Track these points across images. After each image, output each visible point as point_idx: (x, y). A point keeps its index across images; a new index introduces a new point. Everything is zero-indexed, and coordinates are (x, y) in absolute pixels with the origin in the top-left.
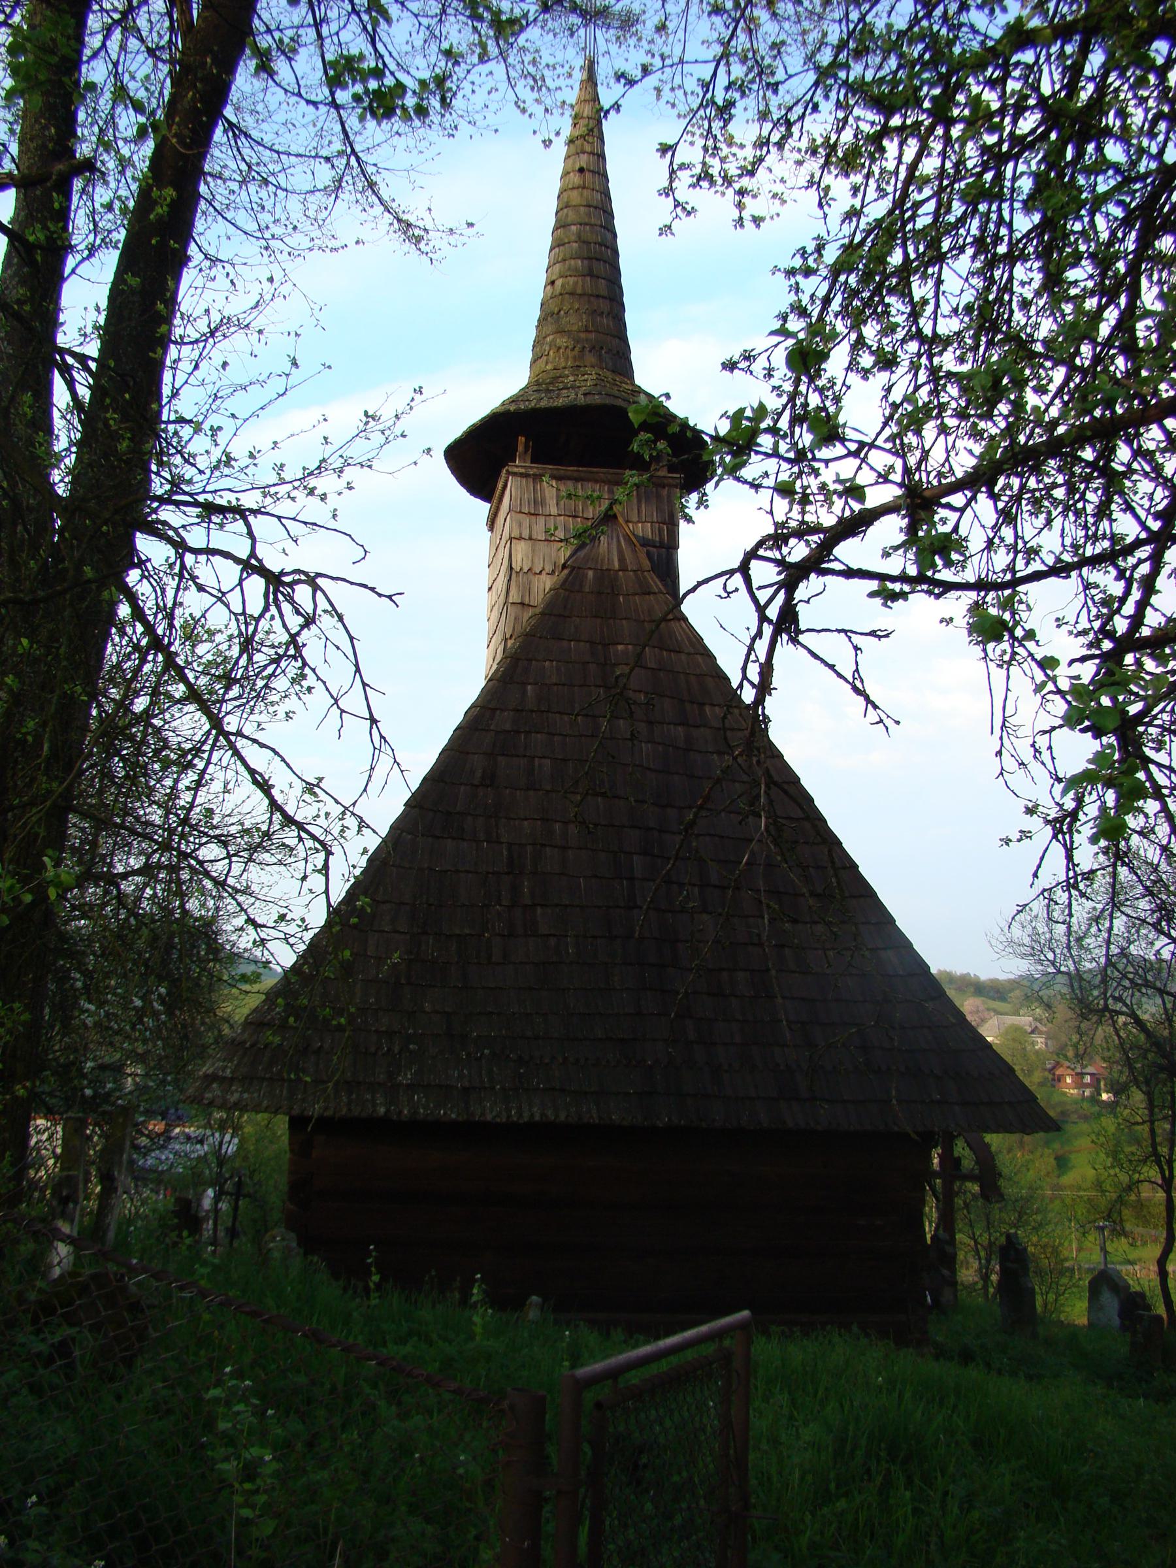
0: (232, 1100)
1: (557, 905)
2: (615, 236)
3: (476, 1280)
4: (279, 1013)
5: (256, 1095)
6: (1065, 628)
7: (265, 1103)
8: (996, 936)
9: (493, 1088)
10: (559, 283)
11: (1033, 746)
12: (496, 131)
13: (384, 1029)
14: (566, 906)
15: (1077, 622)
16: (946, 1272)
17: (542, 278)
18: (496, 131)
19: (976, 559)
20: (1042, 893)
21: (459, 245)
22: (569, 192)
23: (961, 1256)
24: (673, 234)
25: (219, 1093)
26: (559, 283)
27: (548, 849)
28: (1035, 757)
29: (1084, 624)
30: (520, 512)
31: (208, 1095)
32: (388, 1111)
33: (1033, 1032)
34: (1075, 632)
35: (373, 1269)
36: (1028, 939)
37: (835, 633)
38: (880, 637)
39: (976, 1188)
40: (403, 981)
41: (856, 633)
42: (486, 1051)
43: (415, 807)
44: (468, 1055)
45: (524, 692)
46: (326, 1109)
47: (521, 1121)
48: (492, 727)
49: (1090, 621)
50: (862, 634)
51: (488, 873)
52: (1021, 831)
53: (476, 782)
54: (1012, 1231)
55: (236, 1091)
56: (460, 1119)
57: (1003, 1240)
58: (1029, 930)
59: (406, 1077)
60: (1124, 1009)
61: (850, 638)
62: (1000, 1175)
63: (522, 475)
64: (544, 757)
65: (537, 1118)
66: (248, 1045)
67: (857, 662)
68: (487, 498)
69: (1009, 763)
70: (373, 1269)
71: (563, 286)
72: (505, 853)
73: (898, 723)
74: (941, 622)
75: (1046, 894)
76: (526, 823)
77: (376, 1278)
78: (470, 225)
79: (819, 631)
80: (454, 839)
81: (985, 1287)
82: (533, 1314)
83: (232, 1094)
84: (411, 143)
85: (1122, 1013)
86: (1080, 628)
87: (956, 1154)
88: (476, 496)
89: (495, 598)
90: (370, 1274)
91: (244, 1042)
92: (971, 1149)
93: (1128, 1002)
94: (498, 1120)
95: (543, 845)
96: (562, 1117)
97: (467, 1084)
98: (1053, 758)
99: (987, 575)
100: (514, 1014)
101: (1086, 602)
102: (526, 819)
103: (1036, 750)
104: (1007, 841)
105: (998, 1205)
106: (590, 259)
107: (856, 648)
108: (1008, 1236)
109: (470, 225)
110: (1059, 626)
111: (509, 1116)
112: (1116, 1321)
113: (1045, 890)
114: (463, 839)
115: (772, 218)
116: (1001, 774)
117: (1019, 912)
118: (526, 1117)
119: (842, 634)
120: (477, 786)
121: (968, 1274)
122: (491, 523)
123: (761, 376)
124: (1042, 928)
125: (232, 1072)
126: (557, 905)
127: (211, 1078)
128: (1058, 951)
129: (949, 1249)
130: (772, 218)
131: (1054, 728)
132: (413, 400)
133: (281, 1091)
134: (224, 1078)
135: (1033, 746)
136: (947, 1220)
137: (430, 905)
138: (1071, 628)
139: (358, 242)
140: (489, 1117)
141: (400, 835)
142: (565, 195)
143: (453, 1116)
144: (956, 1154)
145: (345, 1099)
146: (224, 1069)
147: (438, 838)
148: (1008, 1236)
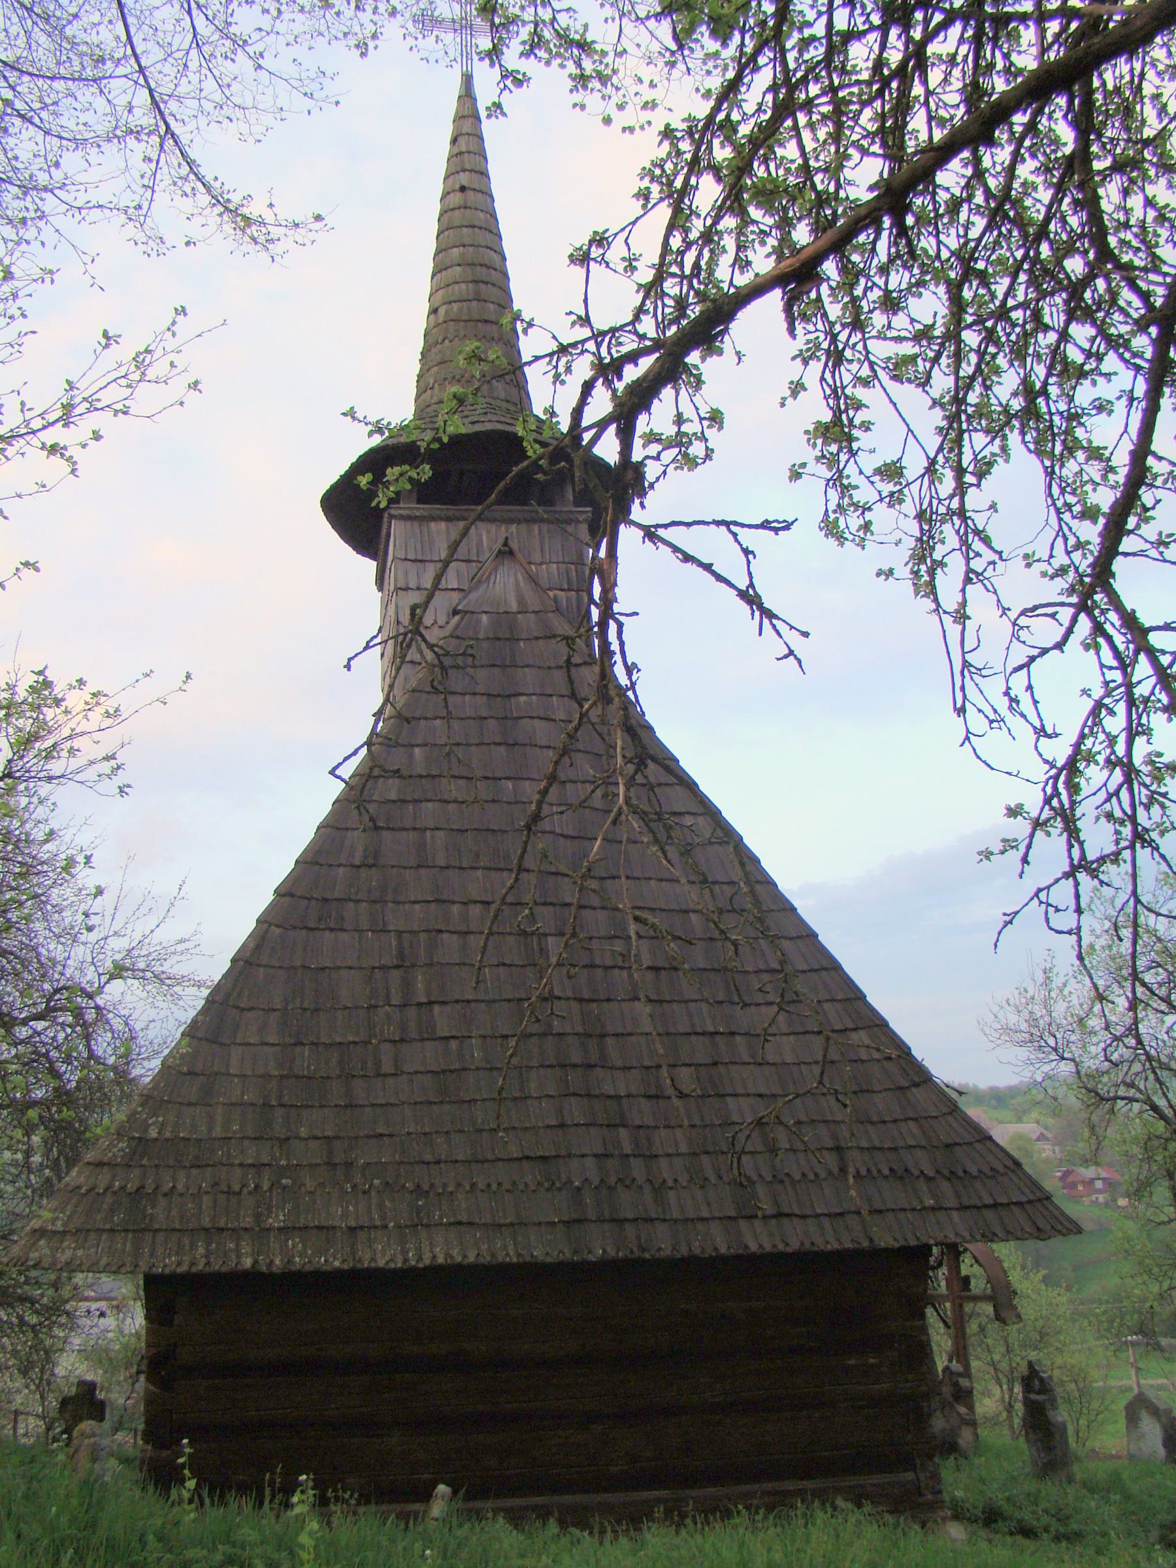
1: (457, 1001)
2: (504, 259)
4: (122, 1150)
5: (93, 1250)
6: (1038, 567)
7: (104, 1261)
9: (385, 1227)
10: (442, 311)
11: (1006, 694)
12: (337, 103)
13: (250, 1161)
15: (1051, 556)
16: (963, 1410)
17: (425, 308)
18: (337, 103)
19: (915, 487)
20: (1036, 895)
22: (449, 213)
23: (978, 1387)
25: (48, 1252)
28: (1010, 708)
30: (406, 559)
32: (256, 1262)
33: (1038, 1139)
34: (1051, 572)
35: (186, 1472)
36: (1026, 1025)
37: (712, 526)
38: (776, 530)
39: (989, 1309)
40: (273, 1103)
41: (743, 526)
42: (376, 1182)
43: (284, 895)
44: (354, 1187)
45: (411, 756)
46: (179, 1264)
48: (375, 798)
49: (1068, 553)
50: (750, 526)
52: (1004, 841)
53: (357, 862)
56: (346, 1267)
57: (1024, 1364)
58: (1025, 1015)
59: (276, 1220)
60: (1138, 1095)
62: (1015, 1293)
63: (409, 518)
65: (441, 1260)
66: (83, 1191)
67: (750, 574)
68: (373, 557)
69: (977, 723)
70: (186, 1472)
71: (447, 313)
72: (394, 943)
73: (805, 634)
74: (878, 575)
75: (1043, 896)
78: (318, 218)
79: (688, 525)
80: (332, 930)
82: (437, 1509)
83: (63, 1252)
86: (1056, 563)
88: (364, 555)
89: (386, 664)
90: (182, 1481)
91: (79, 1187)
93: (1142, 1087)
94: (392, 1265)
95: (440, 931)
96: (471, 1258)
97: (353, 1224)
98: (1035, 702)
100: (409, 1134)
101: (1061, 528)
104: (987, 855)
105: (1016, 1327)
107: (746, 552)
108: (1030, 1364)
109: (318, 218)
110: (1028, 566)
111: (406, 1260)
113: (1040, 890)
115: (642, 128)
116: (967, 738)
117: (1006, 924)
118: (427, 1261)
119: (723, 528)
120: (359, 867)
123: (620, 268)
124: (1039, 1011)
125: (63, 1225)
127: (40, 1233)
129: (964, 1382)
130: (642, 128)
131: (1032, 659)
133: (124, 1245)
134: (55, 1232)
135: (1006, 694)
136: (960, 1352)
138: (1043, 567)
139: (188, 244)
141: (266, 932)
142: (446, 216)
143: (337, 1264)
145: (201, 1251)
147: (311, 929)
148: (1030, 1364)
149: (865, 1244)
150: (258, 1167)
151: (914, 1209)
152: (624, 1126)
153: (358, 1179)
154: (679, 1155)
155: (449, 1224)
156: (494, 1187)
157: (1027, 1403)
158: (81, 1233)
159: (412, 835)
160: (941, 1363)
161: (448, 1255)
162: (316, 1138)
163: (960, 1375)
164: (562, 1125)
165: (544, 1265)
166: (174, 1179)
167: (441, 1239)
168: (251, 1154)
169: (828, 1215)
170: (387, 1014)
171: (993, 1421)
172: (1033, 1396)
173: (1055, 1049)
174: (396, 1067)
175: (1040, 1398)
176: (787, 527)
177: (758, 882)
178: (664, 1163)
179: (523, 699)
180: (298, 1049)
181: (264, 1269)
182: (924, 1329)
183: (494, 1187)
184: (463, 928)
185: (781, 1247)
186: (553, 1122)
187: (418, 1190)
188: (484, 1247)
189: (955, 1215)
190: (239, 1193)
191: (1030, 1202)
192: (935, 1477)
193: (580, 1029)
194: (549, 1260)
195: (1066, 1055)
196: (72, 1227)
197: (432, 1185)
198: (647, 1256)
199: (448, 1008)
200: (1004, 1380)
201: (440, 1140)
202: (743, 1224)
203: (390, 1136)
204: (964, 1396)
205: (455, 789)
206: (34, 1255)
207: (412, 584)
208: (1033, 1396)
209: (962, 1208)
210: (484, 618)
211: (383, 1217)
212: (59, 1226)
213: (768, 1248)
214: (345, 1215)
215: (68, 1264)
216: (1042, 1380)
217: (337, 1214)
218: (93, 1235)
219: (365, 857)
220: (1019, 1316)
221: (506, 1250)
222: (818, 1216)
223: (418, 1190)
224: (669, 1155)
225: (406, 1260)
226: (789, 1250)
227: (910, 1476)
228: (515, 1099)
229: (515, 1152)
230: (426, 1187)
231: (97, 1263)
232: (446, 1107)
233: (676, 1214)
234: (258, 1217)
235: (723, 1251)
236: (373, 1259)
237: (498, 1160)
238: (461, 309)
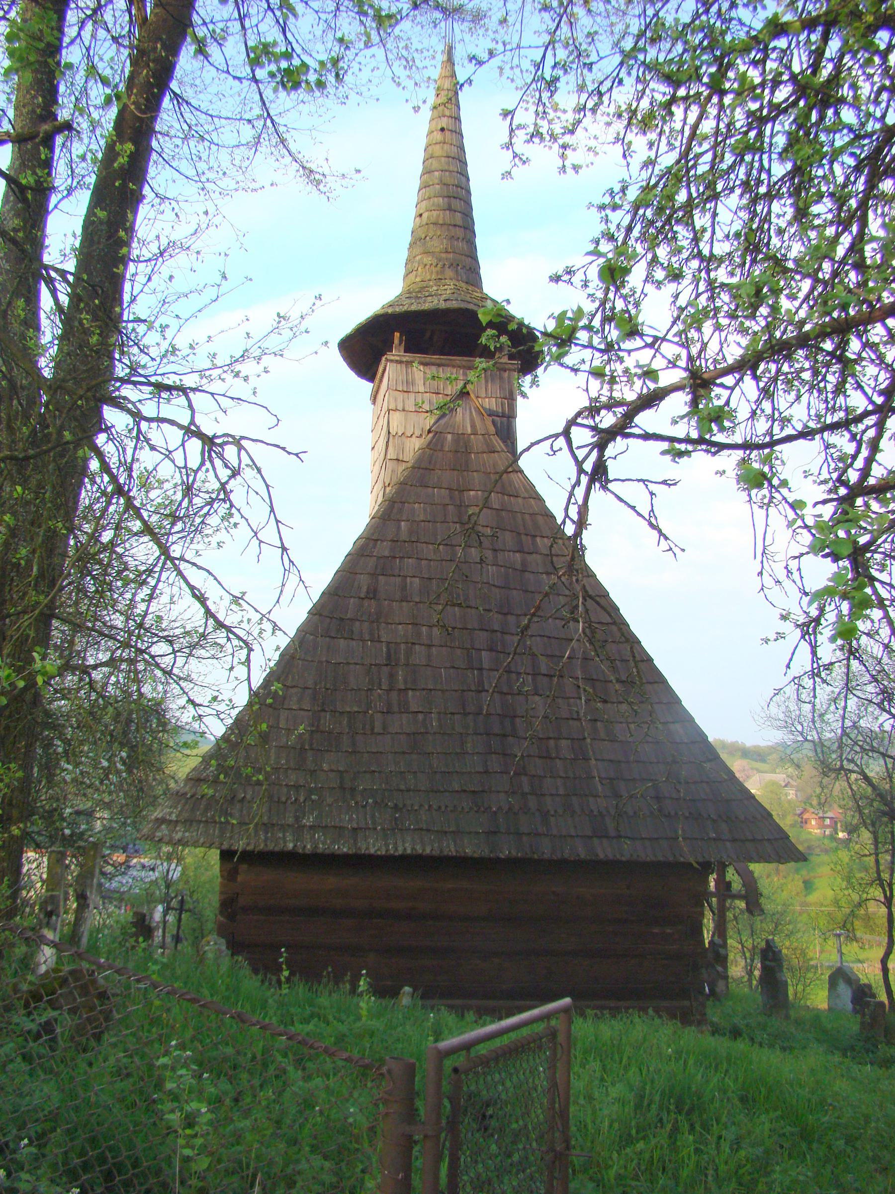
2: (468, 180)
7: (202, 840)
11: (786, 568)
16: (720, 969)
17: (413, 212)
19: (743, 426)
23: (731, 956)
26: (425, 216)
29: (825, 475)
32: (295, 846)
38: (670, 485)
39: (742, 904)
42: (370, 801)
44: (356, 803)
45: (399, 527)
46: (248, 844)
49: (830, 473)
53: (362, 595)
57: (763, 944)
58: (783, 708)
59: (309, 820)
60: (856, 768)
62: (761, 895)
63: (397, 362)
65: (409, 851)
69: (768, 581)
73: (683, 550)
78: (358, 171)
79: (623, 481)
81: (750, 980)
86: (822, 478)
87: (728, 879)
88: (345, 358)
89: (376, 455)
91: (186, 794)
95: (413, 644)
96: (428, 851)
97: (355, 826)
98: (801, 578)
103: (788, 571)
105: (759, 918)
107: (652, 494)
108: (767, 941)
109: (358, 171)
110: (806, 477)
112: (850, 1006)
117: (775, 694)
118: (400, 851)
121: (736, 969)
129: (722, 951)
131: (802, 555)
134: (171, 821)
135: (786, 568)
136: (721, 929)
140: (372, 851)
144: (728, 879)
145: (262, 837)
146: (171, 814)
148: (767, 941)
149: (671, 859)
150: (297, 787)
151: (702, 839)
152: (526, 775)
153: (359, 798)
154: (558, 795)
155: (415, 830)
156: (443, 808)
157: (764, 968)
158: (189, 822)
159: (398, 580)
160: (707, 937)
161: (413, 849)
162: (332, 771)
163: (720, 946)
164: (486, 772)
165: (472, 858)
166: (245, 792)
167: (409, 839)
168: (293, 778)
169: (649, 839)
170: (379, 695)
171: (739, 981)
172: (768, 963)
173: (801, 734)
174: (384, 729)
175: (773, 964)
176: (675, 484)
177: (643, 661)
178: (548, 799)
179: (472, 493)
180: (323, 714)
181: (300, 851)
182: (702, 915)
183: (443, 808)
184: (429, 642)
185: (618, 857)
186: (481, 770)
187: (396, 808)
188: (436, 845)
189: (728, 844)
190: (285, 803)
191: (776, 839)
192: (704, 1006)
193: (500, 712)
194: (476, 855)
195: (809, 738)
196: (181, 818)
197: (404, 805)
198: (536, 856)
199: (418, 693)
200: (748, 955)
201: (410, 777)
202: (596, 841)
203: (380, 772)
204: (722, 960)
205: (427, 551)
206: (159, 834)
207: (400, 407)
208: (768, 963)
209: (734, 840)
210: (449, 437)
211: (374, 823)
212: (174, 817)
213: (611, 857)
214: (351, 819)
215: (179, 841)
216: (774, 952)
217: (348, 820)
218: (194, 824)
219: (368, 592)
220: (762, 910)
221: (450, 848)
222: (642, 839)
223: (396, 808)
224: (552, 795)
225: (387, 851)
226: (624, 859)
227: (686, 1003)
228: (457, 754)
229: (457, 787)
230: (401, 806)
231: (198, 841)
232: (414, 756)
233: (555, 832)
234: (297, 819)
235: (582, 856)
236: (367, 849)
237: (446, 791)
238: (438, 216)
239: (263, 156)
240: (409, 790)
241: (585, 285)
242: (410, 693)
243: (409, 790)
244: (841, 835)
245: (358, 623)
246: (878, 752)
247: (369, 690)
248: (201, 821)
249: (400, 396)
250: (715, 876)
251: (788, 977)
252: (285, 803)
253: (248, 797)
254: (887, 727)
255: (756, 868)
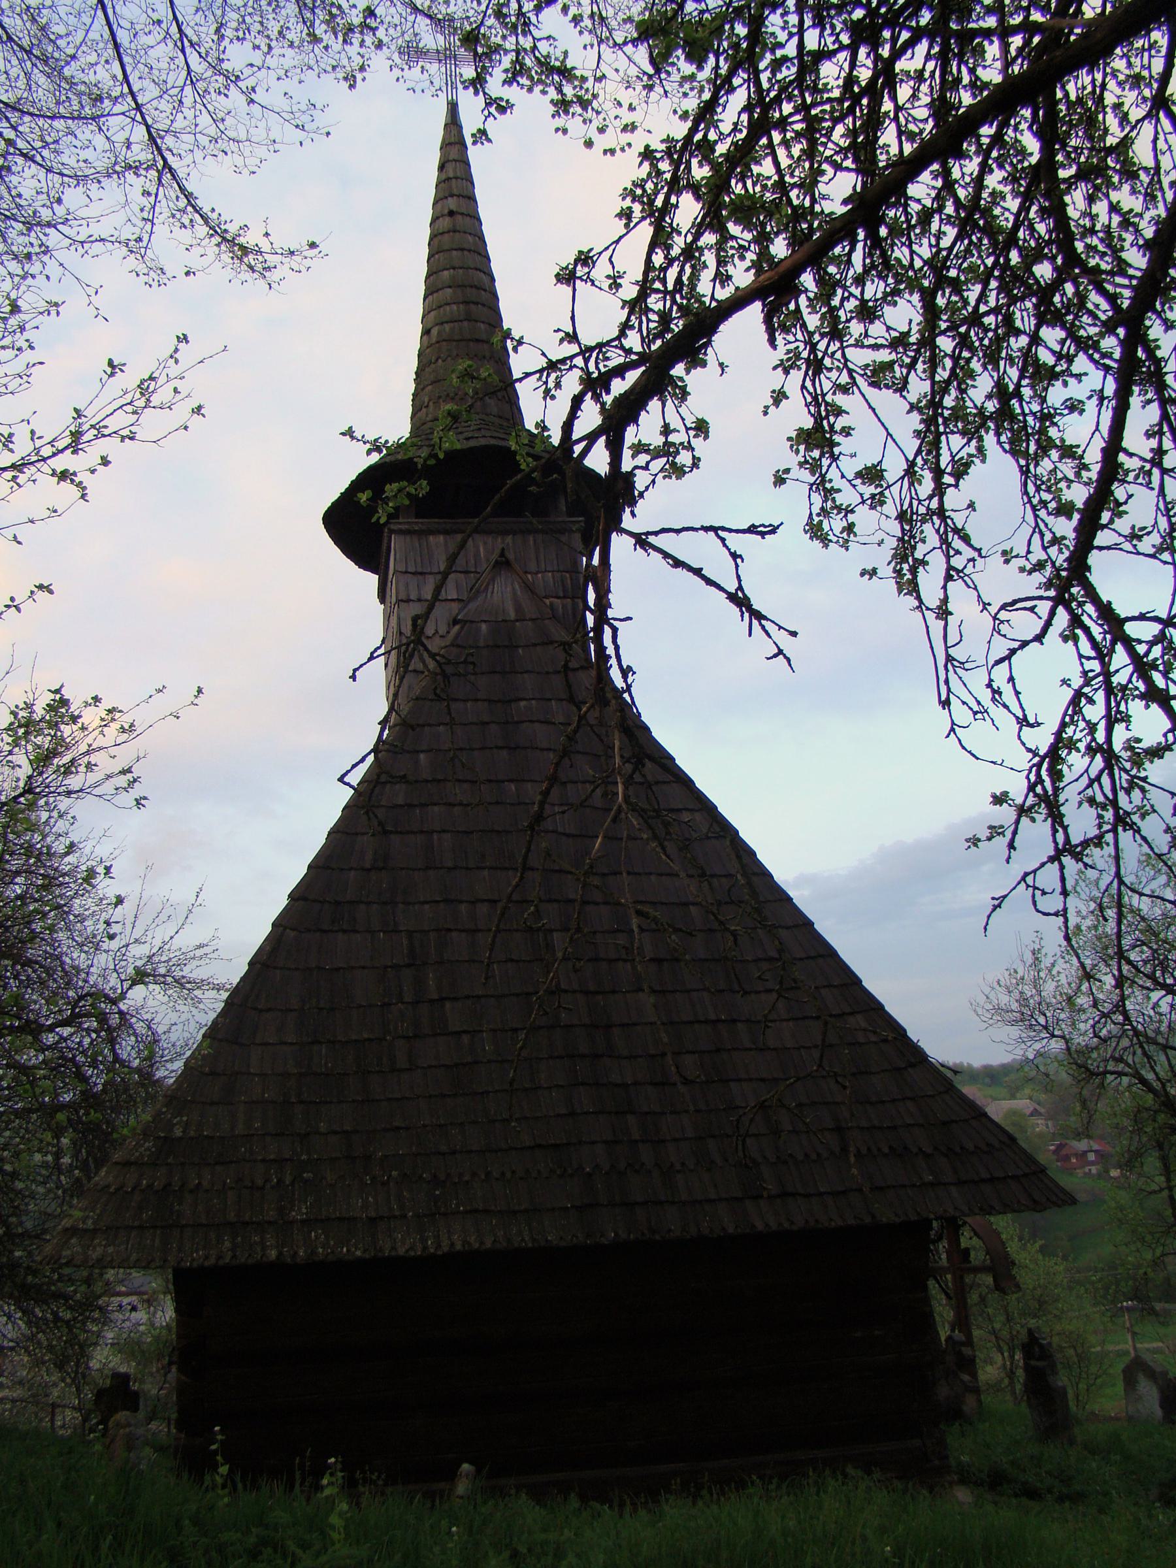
0: (94, 1257)
1: (468, 997)
2: (493, 280)
3: (329, 1467)
4: (148, 1149)
5: (123, 1247)
6: (1016, 563)
7: (134, 1257)
8: (982, 1003)
9: (405, 1216)
10: (435, 331)
11: (989, 686)
12: (328, 134)
13: (272, 1157)
14: (478, 997)
16: (966, 1378)
18: (328, 134)
19: (895, 489)
20: (1023, 879)
21: (303, 269)
24: (489, 141)
25: (80, 1250)
26: (435, 331)
27: (454, 934)
28: (993, 699)
29: (1038, 554)
30: (406, 572)
31: (66, 1252)
32: (280, 1254)
35: (219, 1458)
36: (1016, 1004)
37: (701, 532)
38: (763, 535)
39: (989, 1280)
41: (730, 531)
42: (394, 1173)
44: (373, 1179)
46: (207, 1258)
47: (439, 1253)
49: (1045, 548)
50: (737, 531)
51: (386, 967)
52: (990, 827)
53: (368, 866)
54: (1011, 1458)
55: (100, 1245)
56: (367, 1256)
57: (1024, 1332)
58: (1016, 994)
59: (300, 1212)
60: (1127, 1069)
61: (723, 540)
62: (1013, 1263)
64: (444, 831)
65: (459, 1247)
67: (738, 577)
69: (961, 714)
70: (219, 1458)
71: (439, 333)
73: (794, 634)
74: (862, 575)
76: (427, 907)
77: (224, 1470)
78: (313, 245)
79: (678, 531)
80: (345, 931)
81: (1012, 1383)
82: (461, 1488)
84: (239, 161)
85: (1126, 1075)
86: (1033, 558)
87: (963, 1245)
90: (215, 1467)
91: (108, 1186)
92: (979, 1237)
93: (1130, 1061)
94: (412, 1253)
95: (449, 930)
96: (488, 1244)
97: (373, 1214)
98: (1017, 693)
99: (911, 505)
100: (424, 1126)
102: (427, 902)
103: (994, 692)
106: (466, 303)
107: (735, 556)
108: (1030, 1332)
109: (313, 245)
110: (1007, 562)
111: (425, 1248)
112: (1159, 1413)
114: (357, 932)
115: (623, 150)
116: (952, 730)
117: (995, 908)
119: (712, 534)
120: (369, 870)
121: (990, 1371)
122: (382, 595)
123: (605, 286)
124: (1029, 991)
126: (468, 997)
127: (72, 1231)
128: (1048, 1014)
129: (967, 1351)
130: (623, 150)
131: (1013, 652)
132: (176, 350)
134: (86, 1231)
135: (989, 686)
136: (962, 1322)
137: (322, 1009)
140: (401, 1251)
142: (436, 240)
143: (358, 1253)
144: (963, 1245)
145: (227, 1244)
146: (84, 1221)
147: (325, 932)
148: (1030, 1332)
155: (466, 1212)
156: (508, 1175)
162: (335, 1133)
163: (962, 1344)
172: (1033, 1363)
173: (1046, 1027)
179: (523, 703)
183: (508, 1175)
185: (786, 1225)
186: (563, 1111)
189: (953, 1189)
190: (263, 1188)
191: (1025, 1175)
195: (1056, 1033)
198: (657, 1237)
203: (407, 1128)
204: (968, 1364)
208: (1033, 1363)
210: (484, 626)
212: (90, 1224)
216: (1041, 1346)
222: (821, 1194)
224: (675, 1140)
235: (731, 1230)
236: (394, 1248)
239: (166, 228)
240: (454, 1153)
241: (615, 283)
242: (448, 1005)
243: (454, 1153)
244: (1114, 1173)
245: (363, 907)
246: (1157, 1044)
247: (384, 1005)
248: (133, 1228)
249: (413, 581)
250: (945, 1243)
251: (1062, 1379)
252: (263, 1188)
253: (205, 1184)
254: (1164, 1007)
255: (1004, 1224)
